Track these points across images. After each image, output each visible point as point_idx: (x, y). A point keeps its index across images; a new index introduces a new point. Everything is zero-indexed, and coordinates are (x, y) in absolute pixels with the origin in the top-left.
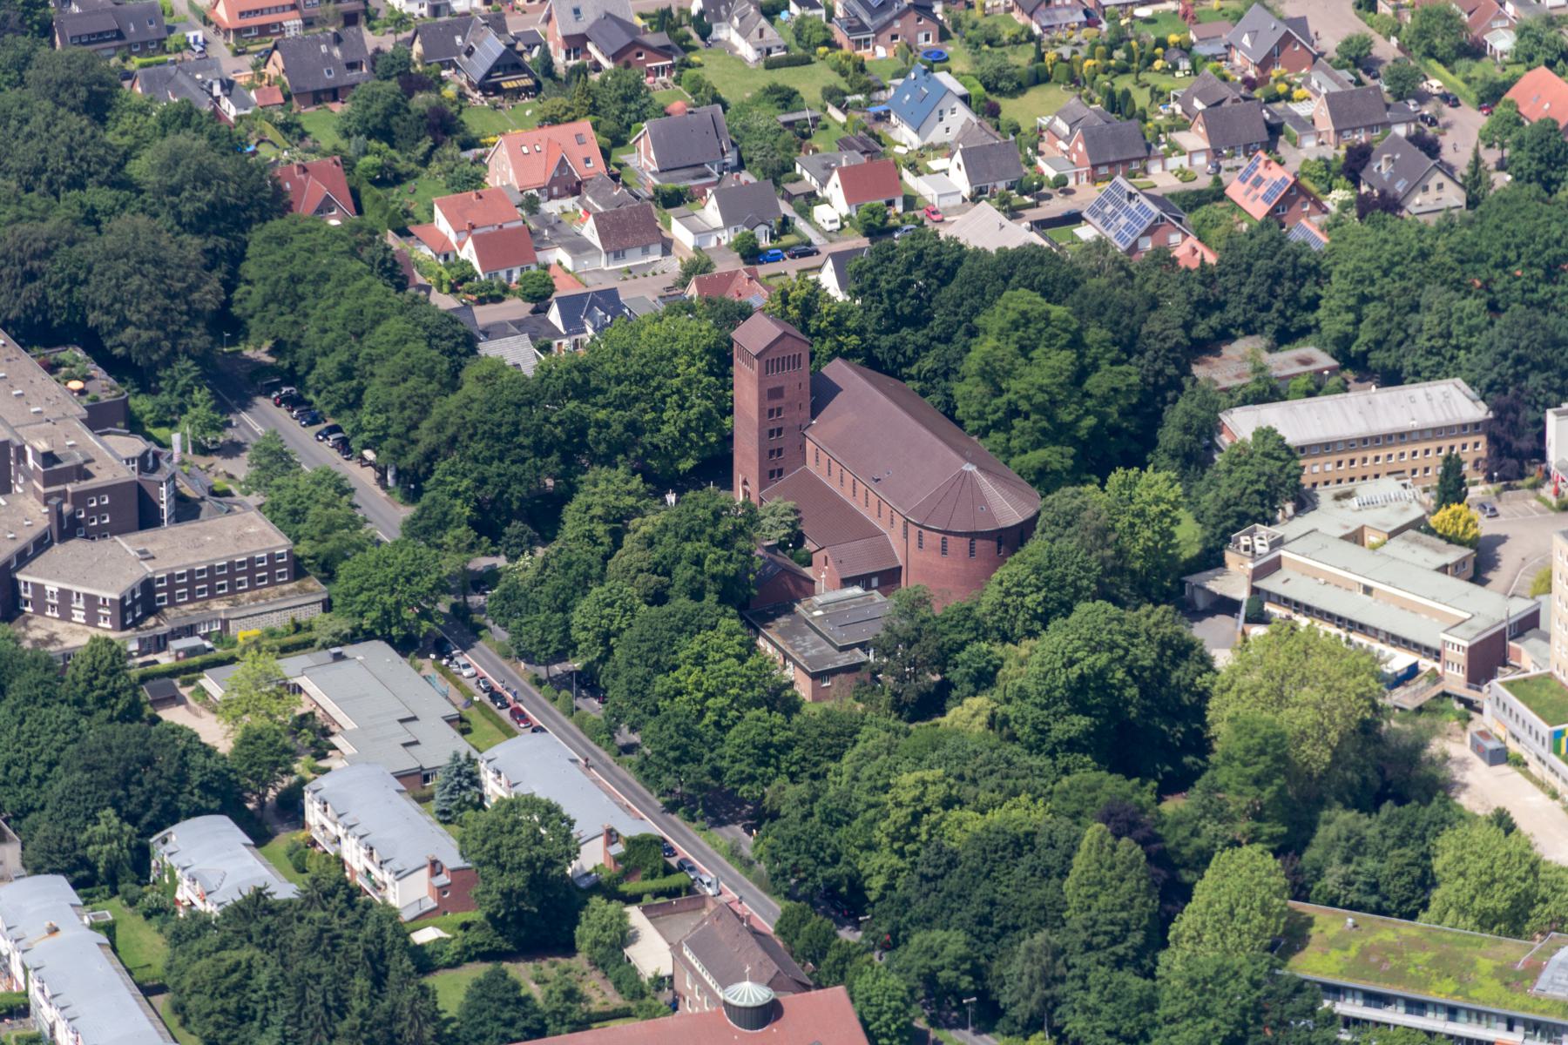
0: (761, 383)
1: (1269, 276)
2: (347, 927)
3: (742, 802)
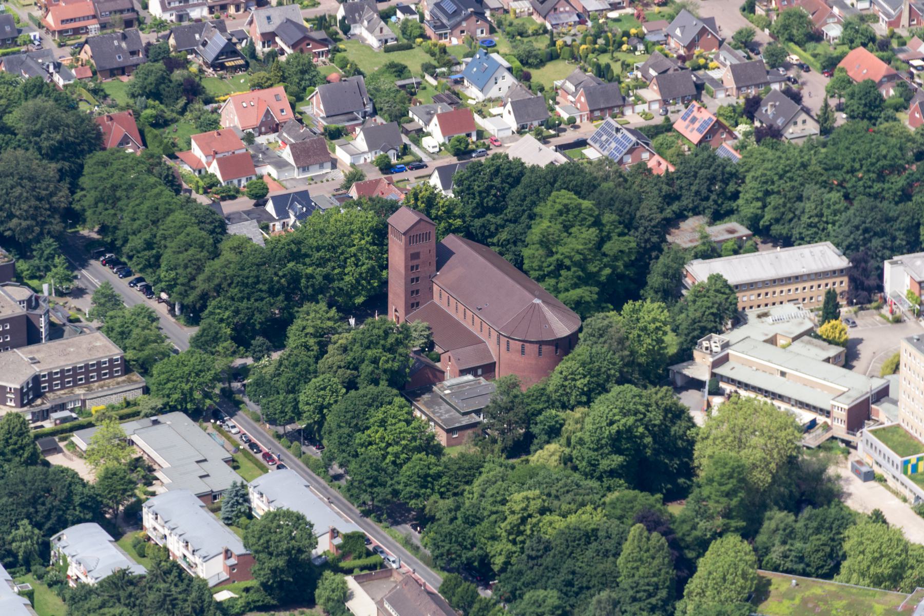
0: (406, 250)
1: (708, 179)
2: (180, 593)
3: (409, 510)
